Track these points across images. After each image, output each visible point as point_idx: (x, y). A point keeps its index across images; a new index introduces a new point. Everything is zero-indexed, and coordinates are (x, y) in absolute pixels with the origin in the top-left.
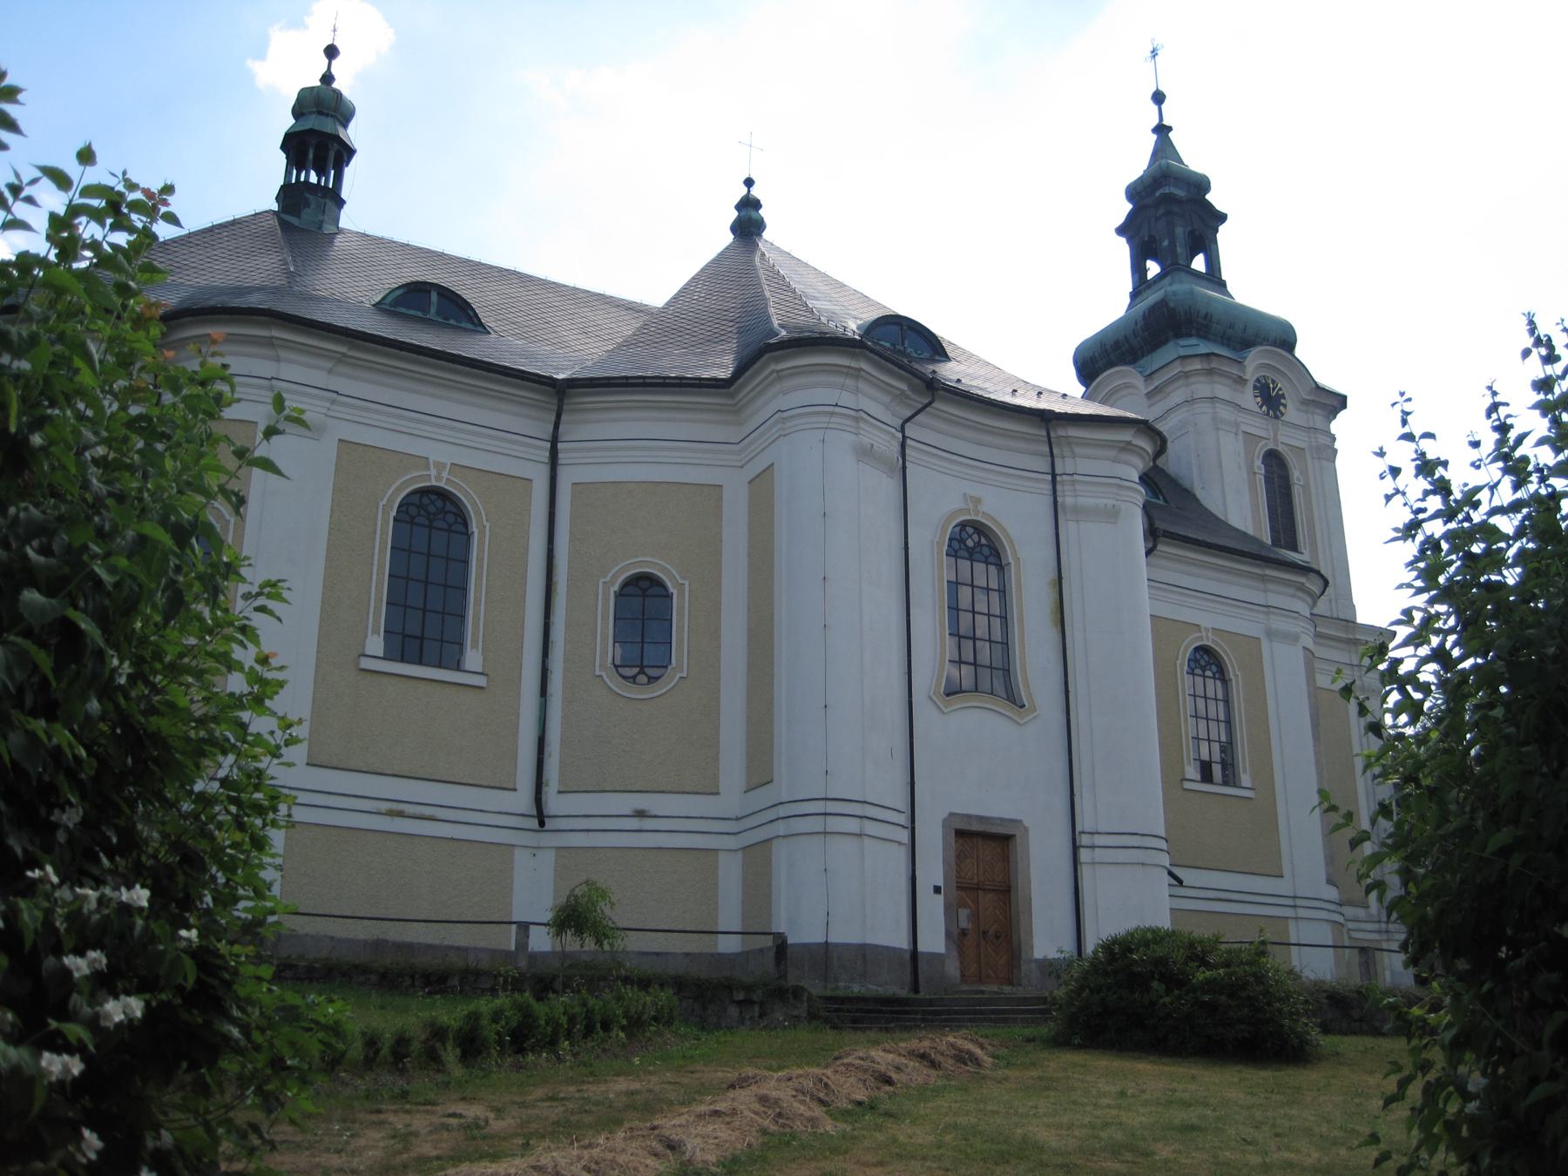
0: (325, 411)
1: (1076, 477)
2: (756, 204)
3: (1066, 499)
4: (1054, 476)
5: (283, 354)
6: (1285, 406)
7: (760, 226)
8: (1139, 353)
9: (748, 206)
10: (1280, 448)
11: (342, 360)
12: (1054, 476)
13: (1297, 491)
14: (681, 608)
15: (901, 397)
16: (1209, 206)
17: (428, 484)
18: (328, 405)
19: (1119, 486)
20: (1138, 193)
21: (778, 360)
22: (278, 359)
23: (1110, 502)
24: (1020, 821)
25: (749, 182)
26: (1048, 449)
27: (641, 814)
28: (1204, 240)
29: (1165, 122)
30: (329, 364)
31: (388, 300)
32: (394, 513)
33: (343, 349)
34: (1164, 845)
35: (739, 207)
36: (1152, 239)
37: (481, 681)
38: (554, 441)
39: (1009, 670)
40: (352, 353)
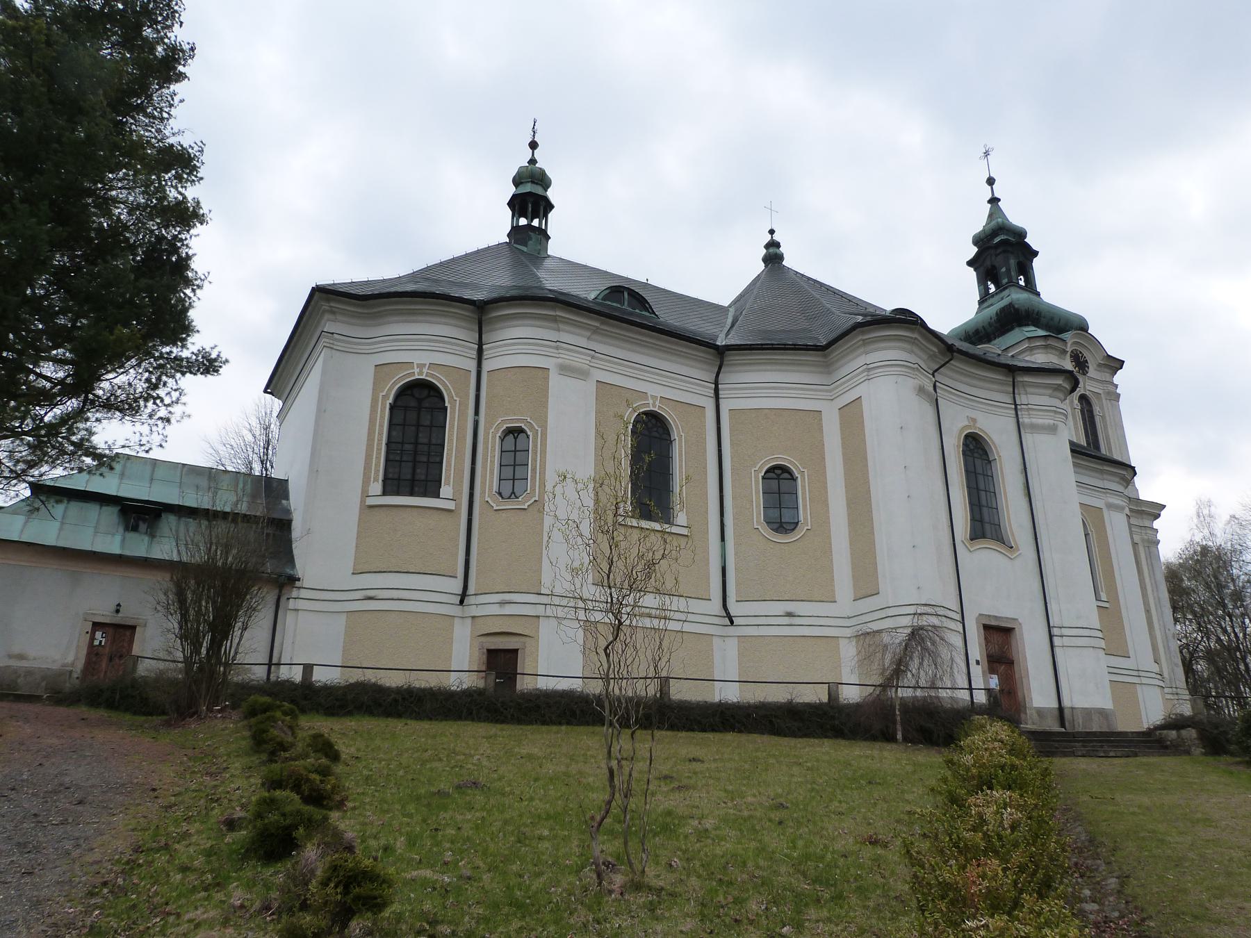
0: (588, 362)
1: (1030, 406)
2: (777, 245)
3: (1025, 420)
4: (1016, 405)
5: (561, 326)
6: (1088, 368)
7: (780, 258)
8: (992, 336)
9: (773, 245)
10: (1087, 393)
11: (596, 331)
12: (1016, 405)
13: (1098, 420)
14: (803, 487)
15: (932, 357)
16: (1028, 246)
17: (648, 409)
18: (589, 358)
19: (1055, 412)
20: (982, 240)
21: (863, 333)
22: (559, 330)
23: (1052, 422)
24: (1017, 619)
25: (772, 232)
26: (1011, 389)
27: (790, 615)
28: (1025, 269)
29: (997, 195)
30: (588, 334)
31: (600, 297)
32: (391, 400)
33: (597, 324)
34: (1099, 634)
35: (768, 246)
36: (994, 267)
37: (685, 531)
38: (716, 384)
39: (999, 525)
40: (602, 327)
